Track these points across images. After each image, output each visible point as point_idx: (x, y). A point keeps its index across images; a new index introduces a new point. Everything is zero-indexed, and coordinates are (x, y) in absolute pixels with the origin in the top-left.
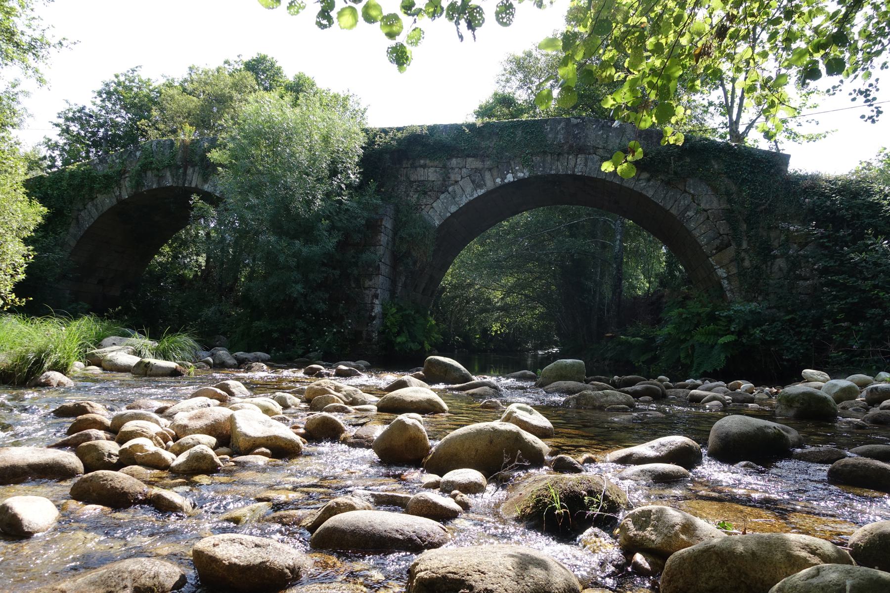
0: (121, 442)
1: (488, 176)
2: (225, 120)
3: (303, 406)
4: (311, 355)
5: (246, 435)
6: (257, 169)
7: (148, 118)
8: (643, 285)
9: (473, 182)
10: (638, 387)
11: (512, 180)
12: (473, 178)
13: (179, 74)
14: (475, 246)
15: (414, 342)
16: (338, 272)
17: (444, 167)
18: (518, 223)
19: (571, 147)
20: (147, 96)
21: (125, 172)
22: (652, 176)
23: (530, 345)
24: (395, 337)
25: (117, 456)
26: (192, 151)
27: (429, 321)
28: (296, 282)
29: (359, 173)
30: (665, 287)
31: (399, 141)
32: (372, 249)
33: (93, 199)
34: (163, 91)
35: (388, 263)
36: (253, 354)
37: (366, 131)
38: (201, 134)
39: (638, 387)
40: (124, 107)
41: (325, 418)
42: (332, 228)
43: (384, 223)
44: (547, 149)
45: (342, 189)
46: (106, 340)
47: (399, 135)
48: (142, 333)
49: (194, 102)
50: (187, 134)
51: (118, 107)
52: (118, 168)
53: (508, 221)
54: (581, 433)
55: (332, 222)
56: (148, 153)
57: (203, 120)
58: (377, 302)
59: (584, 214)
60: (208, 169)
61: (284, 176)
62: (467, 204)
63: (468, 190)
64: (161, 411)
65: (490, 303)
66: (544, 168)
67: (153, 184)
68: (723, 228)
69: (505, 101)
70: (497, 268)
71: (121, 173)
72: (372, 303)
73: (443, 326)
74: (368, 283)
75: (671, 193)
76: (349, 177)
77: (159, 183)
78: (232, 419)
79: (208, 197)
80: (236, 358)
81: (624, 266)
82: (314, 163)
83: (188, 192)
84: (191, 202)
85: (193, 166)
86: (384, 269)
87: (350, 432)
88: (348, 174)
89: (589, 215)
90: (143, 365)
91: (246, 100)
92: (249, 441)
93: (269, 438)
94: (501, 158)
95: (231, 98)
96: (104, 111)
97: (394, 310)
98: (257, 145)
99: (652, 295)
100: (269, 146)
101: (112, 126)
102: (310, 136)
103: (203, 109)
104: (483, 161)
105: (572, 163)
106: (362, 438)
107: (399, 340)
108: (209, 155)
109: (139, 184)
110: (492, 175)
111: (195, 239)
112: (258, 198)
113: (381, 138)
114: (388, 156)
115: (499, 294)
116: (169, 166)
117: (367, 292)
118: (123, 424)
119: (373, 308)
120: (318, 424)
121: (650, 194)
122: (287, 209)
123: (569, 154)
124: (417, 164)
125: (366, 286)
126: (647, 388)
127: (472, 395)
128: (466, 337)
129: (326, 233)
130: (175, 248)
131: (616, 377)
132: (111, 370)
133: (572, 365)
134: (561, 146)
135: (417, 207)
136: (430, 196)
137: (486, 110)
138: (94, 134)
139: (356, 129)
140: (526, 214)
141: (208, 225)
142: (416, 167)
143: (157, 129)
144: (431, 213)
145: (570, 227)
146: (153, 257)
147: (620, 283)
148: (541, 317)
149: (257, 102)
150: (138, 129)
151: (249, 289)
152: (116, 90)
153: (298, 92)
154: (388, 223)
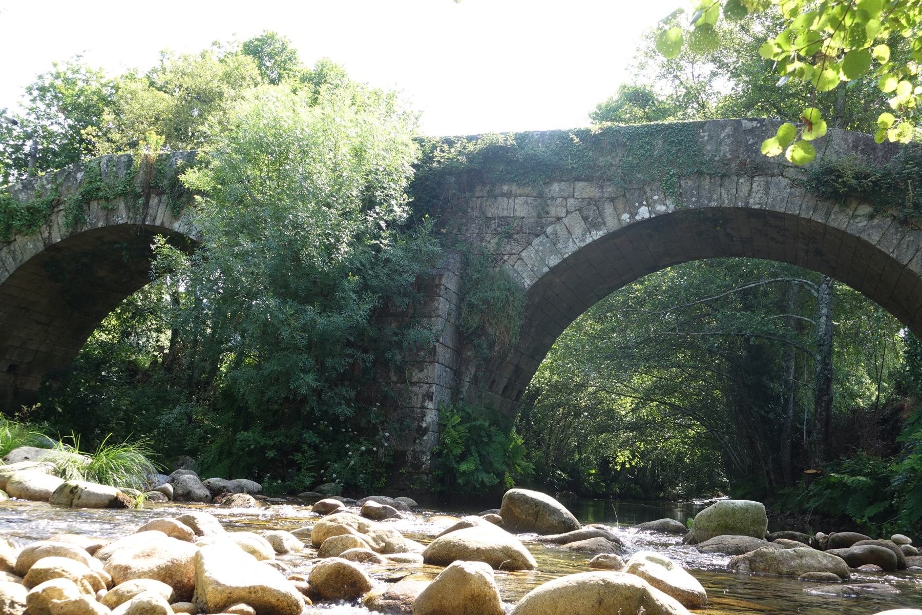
0: (30, 585)
1: (608, 210)
2: (210, 125)
3: (309, 551)
4: (326, 487)
5: (218, 583)
6: (254, 199)
7: (97, 125)
8: (868, 391)
9: (585, 219)
10: (856, 549)
11: (647, 216)
12: (585, 213)
13: (144, 64)
14: (587, 324)
15: (488, 472)
16: (370, 357)
17: (540, 195)
18: (657, 287)
19: (743, 164)
20: (97, 93)
21: (59, 203)
22: (877, 211)
23: (679, 490)
24: (458, 462)
25: (23, 606)
26: (159, 171)
27: (512, 439)
28: (305, 371)
29: (408, 204)
30: (905, 394)
31: (471, 157)
32: (425, 321)
33: (9, 243)
34: (121, 85)
35: (450, 344)
36: (235, 482)
37: (420, 141)
38: (174, 148)
39: (856, 549)
40: (63, 109)
41: (344, 567)
42: (365, 287)
43: (444, 281)
44: (703, 168)
45: (380, 228)
46: (15, 451)
47: (471, 147)
48: (68, 441)
49: (165, 103)
50: (153, 146)
51: (54, 109)
52: (49, 196)
53: (642, 284)
54: (752, 605)
55: (364, 278)
56: (94, 175)
57: (177, 128)
58: (430, 405)
59: (765, 271)
60: (181, 197)
61: (293, 208)
62: (574, 254)
63: (578, 232)
64: (93, 551)
65: (613, 418)
66: (699, 197)
67: (98, 220)
69: (640, 98)
70: (623, 359)
71: (53, 205)
72: (423, 407)
73: (535, 453)
74: (416, 376)
75: (909, 238)
76: (392, 211)
77: (107, 219)
78: (197, 560)
79: (177, 240)
80: (209, 487)
81: (835, 358)
82: (339, 190)
83: (149, 233)
84: (153, 247)
85: (160, 194)
86: (444, 354)
87: (378, 589)
88: (390, 205)
89: (775, 275)
90: (67, 490)
91: (243, 98)
92: (222, 592)
93: (252, 590)
94: (630, 182)
95: (221, 95)
96: (34, 116)
97: (457, 419)
98: (255, 162)
99: (885, 406)
100: (273, 164)
101: (44, 137)
102: (335, 148)
103: (178, 114)
104: (602, 187)
105: (744, 190)
106: (396, 598)
107: (464, 467)
108: (182, 178)
109: (78, 221)
110: (615, 209)
111: (155, 310)
112: (253, 241)
113: (442, 151)
114: (452, 179)
115: (628, 402)
116: (124, 194)
117: (415, 389)
118: (34, 562)
119: (424, 415)
120: (330, 575)
121: (874, 238)
122: (297, 259)
123: (739, 175)
124: (497, 191)
125: (414, 379)
126: (872, 552)
127: (578, 549)
128: (574, 472)
129: (354, 296)
130: (126, 320)
131: (820, 534)
132: (19, 497)
133: (745, 510)
134: (726, 163)
135: (497, 258)
136: (517, 241)
137: (609, 111)
138: (18, 148)
139: (406, 139)
140: (670, 272)
141: (172, 288)
142: (496, 197)
143: (109, 140)
144: (519, 266)
145: (744, 294)
146: (90, 333)
147: (829, 387)
148: (698, 441)
149: (257, 98)
150: (82, 141)
151: (235, 380)
152: (52, 85)
153: (318, 84)
154: (450, 282)
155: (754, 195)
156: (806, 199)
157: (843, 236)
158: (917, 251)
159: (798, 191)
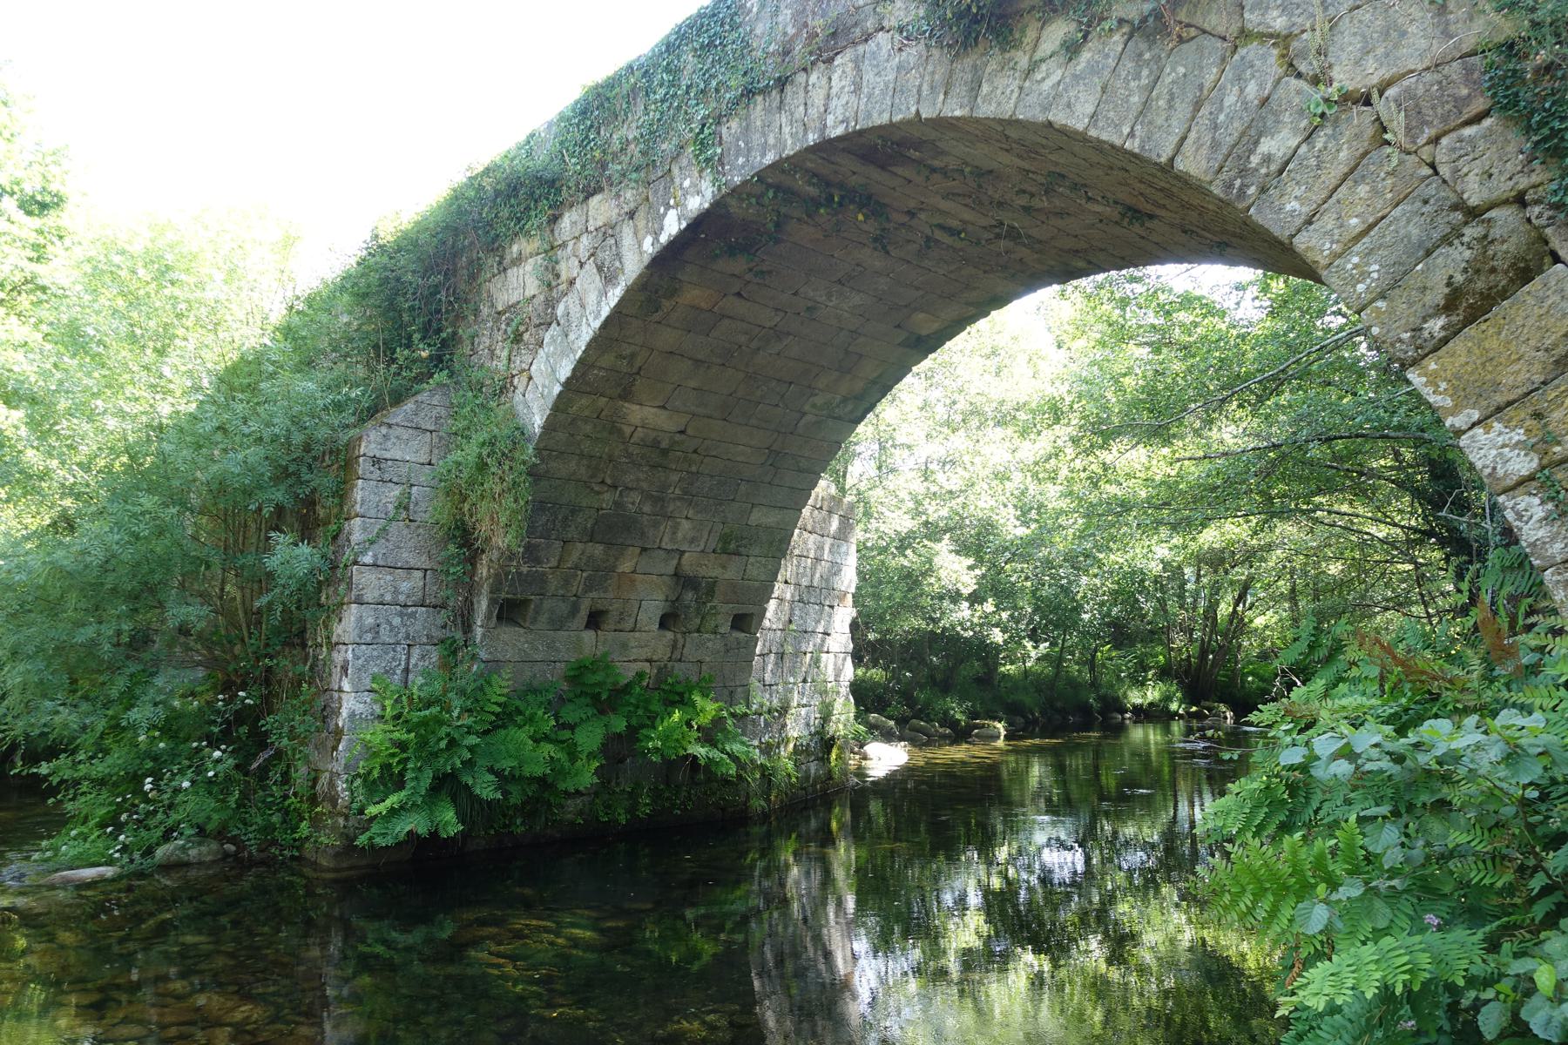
68: (1489, 162)
155: (834, 103)
156: (930, 68)
157: (1004, 131)
158: (1198, 105)
159: (913, 52)
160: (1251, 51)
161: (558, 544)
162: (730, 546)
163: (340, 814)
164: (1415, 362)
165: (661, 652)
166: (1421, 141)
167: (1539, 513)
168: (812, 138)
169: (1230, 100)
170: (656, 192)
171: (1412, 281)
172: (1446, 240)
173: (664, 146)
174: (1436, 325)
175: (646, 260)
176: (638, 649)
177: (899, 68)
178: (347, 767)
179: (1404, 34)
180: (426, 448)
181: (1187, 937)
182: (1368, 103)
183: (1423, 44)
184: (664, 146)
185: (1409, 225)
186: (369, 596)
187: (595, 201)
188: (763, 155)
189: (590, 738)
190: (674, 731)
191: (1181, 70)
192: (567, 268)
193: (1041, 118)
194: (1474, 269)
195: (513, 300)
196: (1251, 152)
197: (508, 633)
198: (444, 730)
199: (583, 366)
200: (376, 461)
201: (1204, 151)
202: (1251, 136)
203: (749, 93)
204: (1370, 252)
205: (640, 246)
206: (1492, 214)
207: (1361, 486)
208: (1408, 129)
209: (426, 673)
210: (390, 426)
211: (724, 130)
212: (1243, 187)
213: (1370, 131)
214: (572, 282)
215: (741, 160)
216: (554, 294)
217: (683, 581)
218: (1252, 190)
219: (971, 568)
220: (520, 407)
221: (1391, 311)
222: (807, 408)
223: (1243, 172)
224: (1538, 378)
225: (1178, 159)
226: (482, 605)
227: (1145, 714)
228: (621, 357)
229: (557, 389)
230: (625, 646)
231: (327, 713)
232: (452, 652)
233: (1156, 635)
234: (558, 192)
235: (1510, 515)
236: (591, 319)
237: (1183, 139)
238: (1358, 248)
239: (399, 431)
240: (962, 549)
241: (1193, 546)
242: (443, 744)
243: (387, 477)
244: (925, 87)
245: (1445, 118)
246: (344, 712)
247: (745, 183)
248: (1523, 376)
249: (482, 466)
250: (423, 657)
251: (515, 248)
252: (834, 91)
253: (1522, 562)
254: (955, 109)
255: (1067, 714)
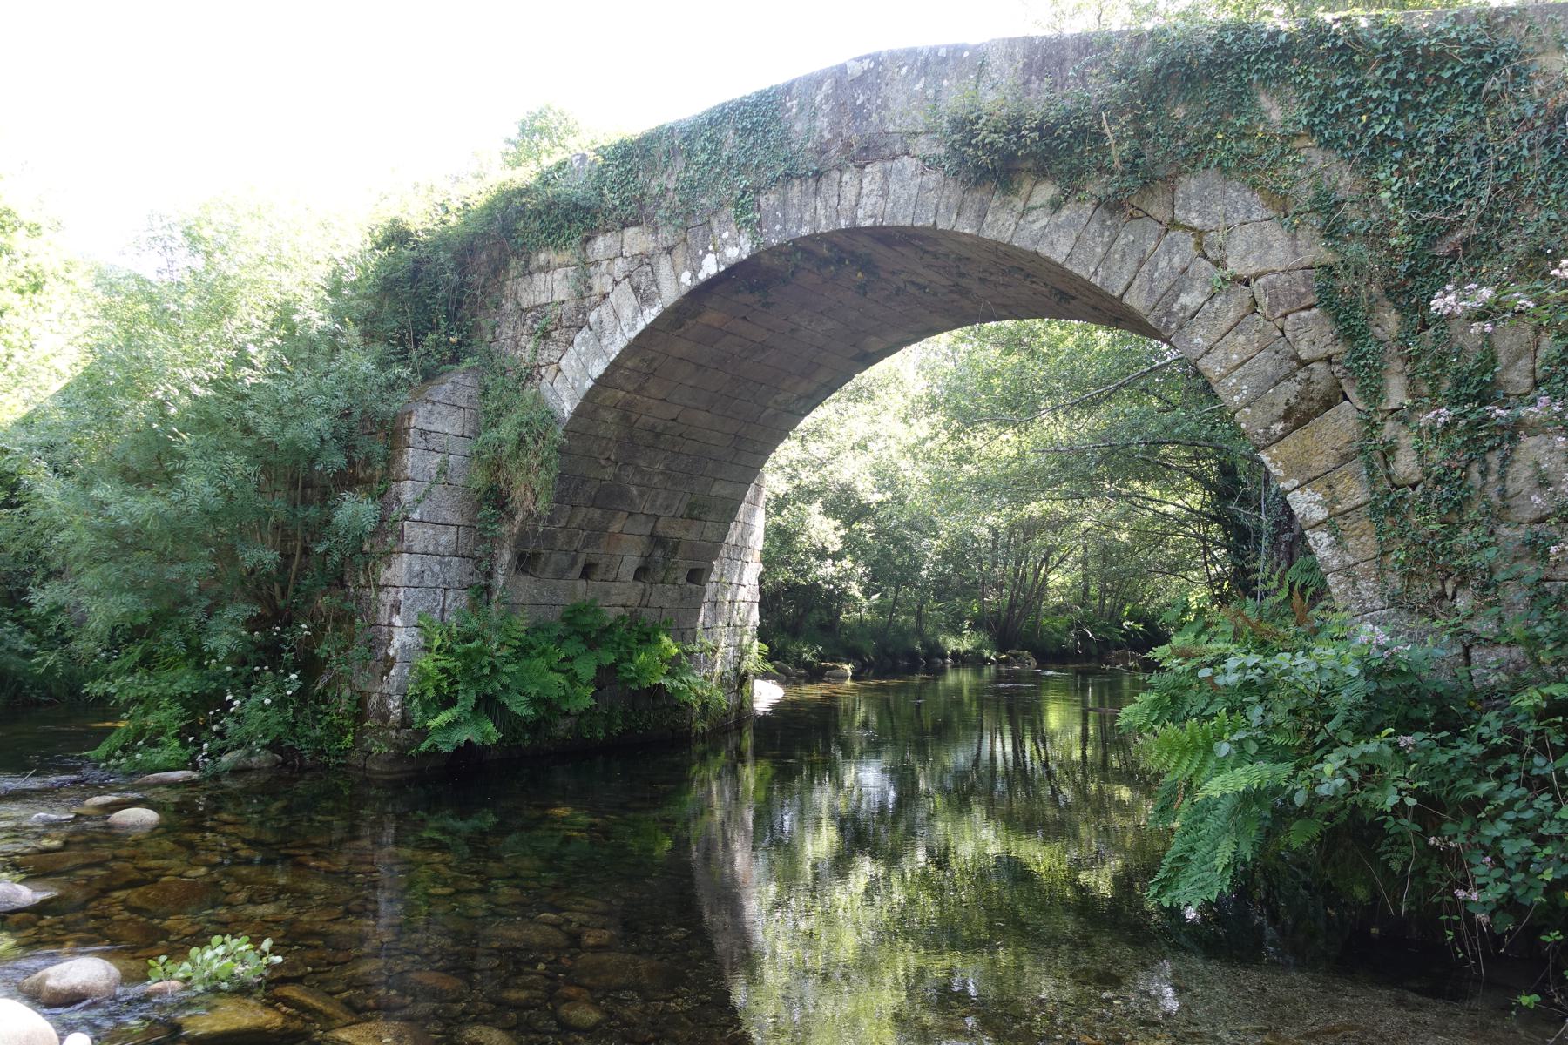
68: (1313, 335)
155: (864, 201)
158: (1141, 263)
159: (932, 178)
160: (1177, 235)
161: (568, 508)
162: (694, 513)
163: (391, 728)
164: (1265, 448)
165: (633, 600)
166: (1277, 314)
167: (1327, 542)
168: (844, 224)
169: (1163, 264)
170: (695, 236)
171: (1266, 399)
172: (1287, 378)
173: (703, 201)
174: (1278, 427)
175: (684, 291)
176: (618, 595)
177: (921, 187)
178: (398, 688)
179: (1271, 247)
180: (460, 423)
181: (994, 849)
182: (1247, 284)
183: (1282, 255)
184: (703, 201)
185: (1266, 364)
186: (416, 548)
187: (630, 232)
188: (800, 227)
189: (586, 669)
190: (649, 665)
191: (1131, 238)
192: (600, 284)
193: (1031, 249)
194: (1301, 396)
195: (541, 300)
196: (1174, 301)
197: (525, 581)
198: (486, 659)
199: (614, 366)
200: (423, 433)
201: (1144, 294)
202: (1175, 290)
203: (789, 177)
204: (1243, 377)
205: (677, 278)
206: (1313, 366)
207: (1154, 469)
208: (1270, 306)
209: (459, 612)
210: (434, 403)
211: (762, 200)
212: (1168, 323)
213: (1248, 303)
214: (605, 296)
215: (778, 227)
216: (586, 302)
217: (656, 540)
218: (1173, 326)
219: (836, 529)
220: (548, 394)
221: (1253, 415)
222: (770, 403)
223: (1168, 313)
224: (1332, 465)
225: (1126, 296)
226: (506, 556)
227: (960, 660)
228: (643, 360)
229: (589, 384)
230: (607, 593)
231: (377, 642)
232: (482, 592)
233: (972, 589)
234: (594, 217)
235: (1311, 542)
236: (626, 330)
237: (1130, 284)
238: (1236, 373)
239: (440, 407)
240: (830, 510)
241: (1018, 515)
242: (486, 671)
243: (431, 446)
244: (942, 206)
245: (1291, 304)
246: (396, 643)
247: (781, 245)
248: (1323, 463)
249: (521, 442)
250: (455, 599)
251: (542, 257)
252: (864, 191)
253: (1313, 568)
254: (966, 227)
255: (896, 657)
